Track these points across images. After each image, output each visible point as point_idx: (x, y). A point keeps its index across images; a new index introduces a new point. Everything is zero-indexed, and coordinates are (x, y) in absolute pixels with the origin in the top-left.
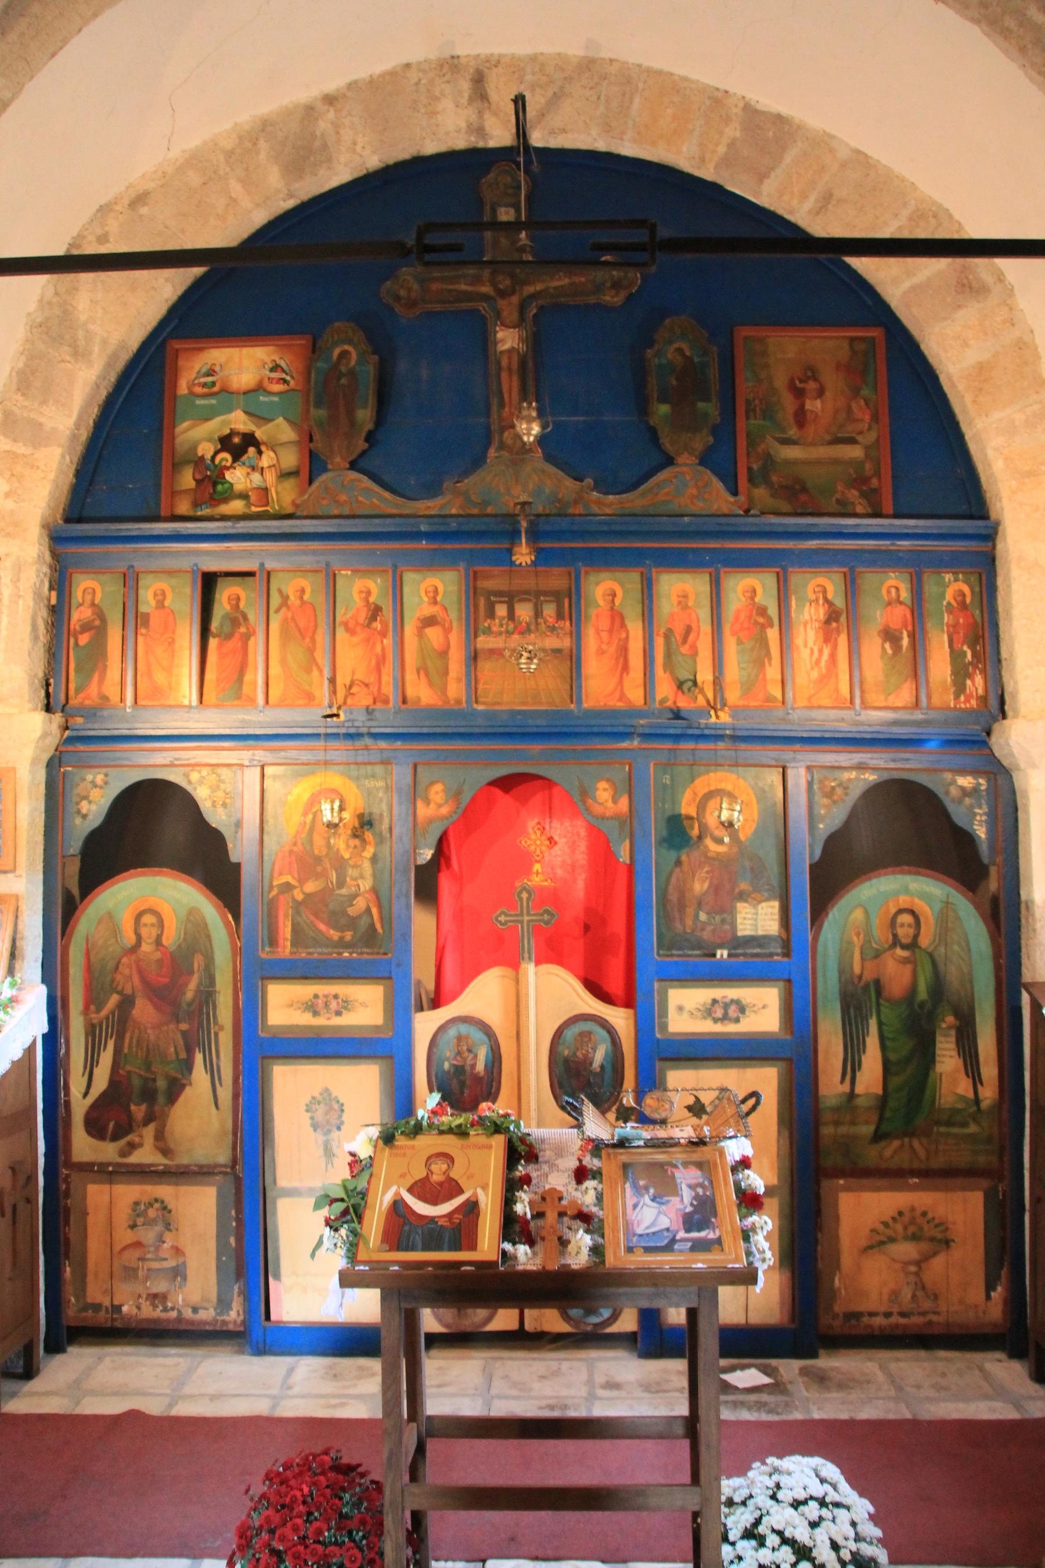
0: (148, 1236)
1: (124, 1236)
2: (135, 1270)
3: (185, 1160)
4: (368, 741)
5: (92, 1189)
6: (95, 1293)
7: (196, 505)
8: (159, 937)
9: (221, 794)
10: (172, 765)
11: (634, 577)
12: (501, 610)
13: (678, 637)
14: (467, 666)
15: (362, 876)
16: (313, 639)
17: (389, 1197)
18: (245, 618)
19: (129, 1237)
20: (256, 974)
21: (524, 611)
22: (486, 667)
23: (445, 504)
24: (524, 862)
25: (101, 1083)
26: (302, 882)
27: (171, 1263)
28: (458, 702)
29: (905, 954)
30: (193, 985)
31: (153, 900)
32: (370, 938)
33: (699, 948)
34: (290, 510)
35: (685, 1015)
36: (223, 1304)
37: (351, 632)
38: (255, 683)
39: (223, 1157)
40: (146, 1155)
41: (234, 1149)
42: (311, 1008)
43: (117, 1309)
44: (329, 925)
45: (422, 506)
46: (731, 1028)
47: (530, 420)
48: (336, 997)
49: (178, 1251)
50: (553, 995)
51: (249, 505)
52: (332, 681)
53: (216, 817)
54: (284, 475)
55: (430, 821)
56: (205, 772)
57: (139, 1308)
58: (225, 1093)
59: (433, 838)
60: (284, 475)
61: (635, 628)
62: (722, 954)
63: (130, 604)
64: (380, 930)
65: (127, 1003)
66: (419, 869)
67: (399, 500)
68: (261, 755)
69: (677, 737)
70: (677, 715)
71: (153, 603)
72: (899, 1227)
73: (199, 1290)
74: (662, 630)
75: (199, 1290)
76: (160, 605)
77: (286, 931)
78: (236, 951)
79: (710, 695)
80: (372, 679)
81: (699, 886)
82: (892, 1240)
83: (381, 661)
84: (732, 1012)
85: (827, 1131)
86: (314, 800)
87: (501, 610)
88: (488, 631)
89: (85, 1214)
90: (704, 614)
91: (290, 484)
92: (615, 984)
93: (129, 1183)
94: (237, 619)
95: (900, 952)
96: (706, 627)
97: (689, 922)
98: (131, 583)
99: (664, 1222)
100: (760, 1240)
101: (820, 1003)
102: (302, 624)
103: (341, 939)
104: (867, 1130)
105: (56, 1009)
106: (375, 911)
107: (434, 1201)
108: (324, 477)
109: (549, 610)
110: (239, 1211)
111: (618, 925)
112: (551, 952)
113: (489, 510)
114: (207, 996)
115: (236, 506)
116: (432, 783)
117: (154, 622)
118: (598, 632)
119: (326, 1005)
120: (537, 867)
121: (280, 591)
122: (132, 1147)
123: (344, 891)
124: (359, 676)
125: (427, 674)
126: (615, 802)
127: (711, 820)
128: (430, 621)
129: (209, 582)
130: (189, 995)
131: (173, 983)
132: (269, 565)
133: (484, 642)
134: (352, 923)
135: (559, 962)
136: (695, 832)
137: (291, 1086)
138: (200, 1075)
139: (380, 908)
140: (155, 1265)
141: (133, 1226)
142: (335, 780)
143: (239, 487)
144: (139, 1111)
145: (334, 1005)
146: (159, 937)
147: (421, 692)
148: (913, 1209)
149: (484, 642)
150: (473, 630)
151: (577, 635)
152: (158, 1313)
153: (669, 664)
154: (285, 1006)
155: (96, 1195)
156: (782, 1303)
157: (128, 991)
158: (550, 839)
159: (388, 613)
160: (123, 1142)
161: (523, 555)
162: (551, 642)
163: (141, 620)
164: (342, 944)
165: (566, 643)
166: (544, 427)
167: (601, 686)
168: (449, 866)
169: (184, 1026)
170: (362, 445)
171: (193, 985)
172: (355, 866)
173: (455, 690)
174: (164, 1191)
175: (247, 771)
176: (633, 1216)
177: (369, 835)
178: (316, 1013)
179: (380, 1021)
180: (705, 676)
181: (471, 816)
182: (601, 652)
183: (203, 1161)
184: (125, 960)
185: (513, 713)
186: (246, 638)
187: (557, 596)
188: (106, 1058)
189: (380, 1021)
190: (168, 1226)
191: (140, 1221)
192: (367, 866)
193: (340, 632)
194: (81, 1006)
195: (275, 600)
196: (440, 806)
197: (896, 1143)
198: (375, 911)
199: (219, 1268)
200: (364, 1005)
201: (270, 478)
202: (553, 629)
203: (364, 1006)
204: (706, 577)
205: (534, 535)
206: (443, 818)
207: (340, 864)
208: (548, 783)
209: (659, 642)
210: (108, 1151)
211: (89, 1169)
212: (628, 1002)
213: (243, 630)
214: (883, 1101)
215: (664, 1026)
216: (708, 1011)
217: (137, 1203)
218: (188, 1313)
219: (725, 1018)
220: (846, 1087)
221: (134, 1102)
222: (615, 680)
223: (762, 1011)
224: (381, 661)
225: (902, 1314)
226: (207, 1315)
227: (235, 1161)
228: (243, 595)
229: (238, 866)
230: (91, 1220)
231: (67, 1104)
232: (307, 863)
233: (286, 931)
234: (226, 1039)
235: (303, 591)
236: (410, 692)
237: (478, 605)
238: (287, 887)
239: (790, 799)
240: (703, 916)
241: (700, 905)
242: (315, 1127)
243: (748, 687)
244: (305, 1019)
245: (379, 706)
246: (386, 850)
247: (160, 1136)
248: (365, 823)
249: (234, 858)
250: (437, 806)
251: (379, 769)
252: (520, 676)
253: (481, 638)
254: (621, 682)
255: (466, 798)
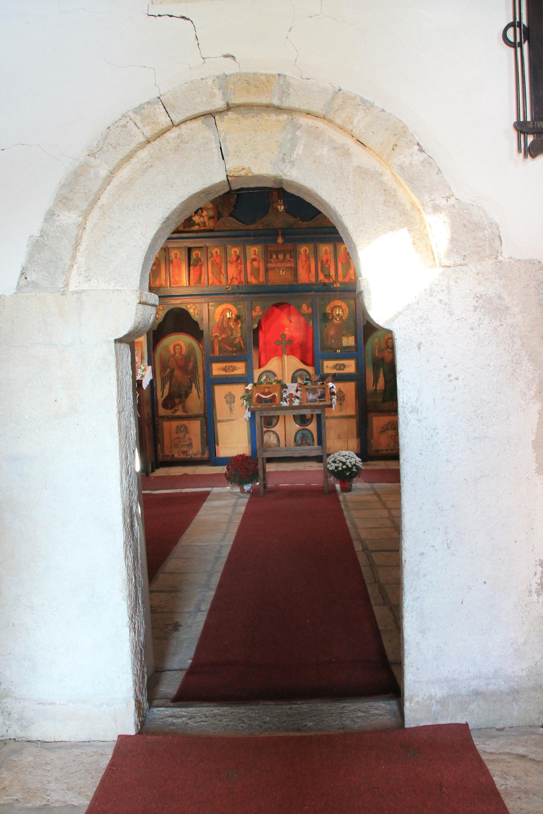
0: (181, 435)
1: (175, 436)
2: (178, 445)
3: (190, 413)
4: (238, 295)
5: (165, 423)
6: (167, 452)
7: (184, 227)
8: (181, 352)
9: (196, 311)
10: (182, 303)
11: (312, 246)
12: (274, 256)
13: (325, 263)
14: (265, 273)
15: (237, 333)
16: (221, 266)
17: (256, 395)
18: (200, 260)
19: (176, 436)
20: (209, 360)
21: (281, 256)
22: (271, 273)
23: (258, 226)
24: (283, 328)
25: (166, 393)
26: (221, 335)
27: (188, 442)
28: (263, 282)
29: (390, 350)
30: (191, 365)
31: (179, 342)
32: (240, 350)
33: (332, 350)
34: (212, 228)
35: (329, 368)
36: (203, 453)
37: (232, 263)
38: (205, 279)
39: (202, 412)
40: (180, 413)
41: (205, 409)
42: (225, 369)
43: (174, 456)
44: (229, 346)
45: (251, 227)
46: (341, 372)
47: (281, 205)
48: (232, 366)
49: (190, 439)
50: (292, 363)
51: (200, 227)
52: (227, 278)
53: (196, 318)
54: (210, 218)
55: (256, 316)
56: (191, 305)
57: (179, 455)
58: (201, 394)
59: (257, 321)
60: (210, 218)
61: (313, 261)
62: (338, 351)
63: (167, 258)
64: (243, 347)
65: (172, 371)
66: (254, 330)
67: (244, 225)
68: (207, 300)
69: (324, 291)
70: (325, 284)
71: (174, 257)
72: (390, 426)
73: (196, 449)
74: (320, 261)
75: (196, 449)
76: (176, 257)
77: (217, 348)
78: (203, 355)
79: (334, 279)
80: (238, 277)
81: (332, 332)
82: (388, 430)
83: (240, 271)
84: (342, 367)
85: (369, 400)
86: (224, 311)
87: (274, 256)
88: (271, 262)
89: (163, 430)
90: (332, 256)
91: (212, 221)
92: (310, 360)
93: (174, 421)
94: (198, 260)
95: (389, 350)
96: (333, 260)
97: (329, 342)
98: (167, 251)
99: (314, 398)
100: (334, 400)
101: (367, 365)
102: (217, 262)
103: (233, 350)
104: (380, 399)
105: (154, 372)
106: (242, 342)
107: (266, 395)
108: (222, 219)
109: (288, 256)
110: (207, 427)
111: (310, 345)
112: (292, 352)
113: (270, 227)
114: (195, 367)
115: (196, 228)
116: (257, 306)
117: (174, 262)
118: (302, 262)
119: (229, 369)
120: (287, 329)
121: (211, 252)
122: (176, 411)
123: (233, 337)
124: (234, 276)
125: (254, 275)
126: (308, 309)
127: (335, 314)
128: (254, 260)
129: (190, 250)
130: (190, 368)
131: (186, 364)
132: (207, 245)
133: (269, 265)
134: (235, 346)
135: (294, 355)
136: (331, 317)
137: (220, 392)
138: (194, 390)
139: (243, 341)
140: (184, 443)
141: (177, 433)
142: (229, 306)
143: (197, 222)
144: (177, 401)
145: (231, 368)
146: (181, 352)
147: (252, 280)
148: (393, 421)
149: (269, 265)
150: (266, 262)
151: (296, 263)
152: (185, 456)
153: (322, 271)
154: (217, 369)
155: (166, 425)
156: (357, 446)
157: (173, 367)
158: (290, 321)
159: (242, 256)
160: (173, 410)
161: (280, 240)
162: (289, 265)
163: (171, 262)
164: (233, 352)
165: (293, 265)
166: (285, 207)
167: (303, 277)
168: (262, 329)
169: (189, 377)
170: (232, 209)
171: (191, 365)
172: (236, 330)
173: (262, 279)
174: (185, 423)
175: (204, 304)
176: (308, 397)
177: (239, 321)
178: (226, 371)
179: (244, 373)
180: (332, 273)
181: (267, 316)
182: (303, 267)
183: (197, 413)
184: (171, 359)
185: (279, 285)
186: (201, 266)
187: (290, 252)
188: (167, 386)
189: (244, 373)
190: (187, 433)
191: (179, 431)
192: (239, 329)
193: (229, 264)
194: (159, 373)
195: (209, 255)
196: (259, 312)
197: (388, 403)
198: (242, 342)
199: (201, 443)
200: (239, 368)
201: (206, 219)
202: (289, 261)
203: (240, 369)
204: (332, 245)
205: (283, 235)
206: (259, 316)
207: (231, 330)
208: (290, 305)
209: (319, 264)
210: (169, 412)
211: (163, 417)
212: (313, 365)
213: (200, 263)
214: (385, 391)
215: (323, 371)
216: (335, 367)
217: (177, 426)
218: (193, 456)
219: (340, 369)
220: (374, 388)
221: (176, 398)
222: (307, 276)
223: (350, 367)
224: (240, 271)
225: (391, 450)
226: (199, 456)
227: (205, 414)
228: (199, 253)
229: (203, 331)
230: (165, 432)
231: (157, 400)
232: (222, 329)
233: (217, 348)
234: (201, 379)
235: (217, 252)
236: (249, 280)
237: (267, 255)
238: (217, 337)
239: (357, 307)
240: (333, 341)
241: (332, 338)
242: (227, 403)
243: (344, 276)
244: (223, 373)
245: (240, 284)
246: (244, 325)
247: (184, 407)
248: (238, 318)
249: (201, 329)
250: (258, 312)
251: (242, 303)
252: (280, 275)
253: (269, 264)
254: (308, 276)
255: (266, 310)
